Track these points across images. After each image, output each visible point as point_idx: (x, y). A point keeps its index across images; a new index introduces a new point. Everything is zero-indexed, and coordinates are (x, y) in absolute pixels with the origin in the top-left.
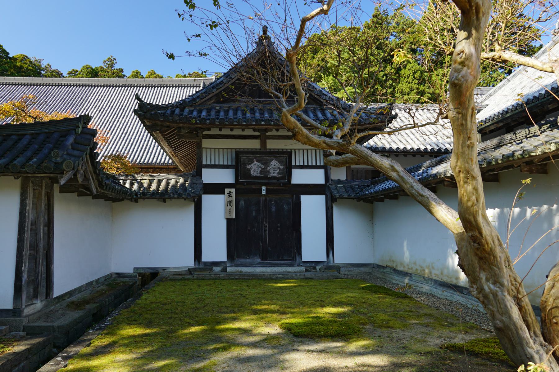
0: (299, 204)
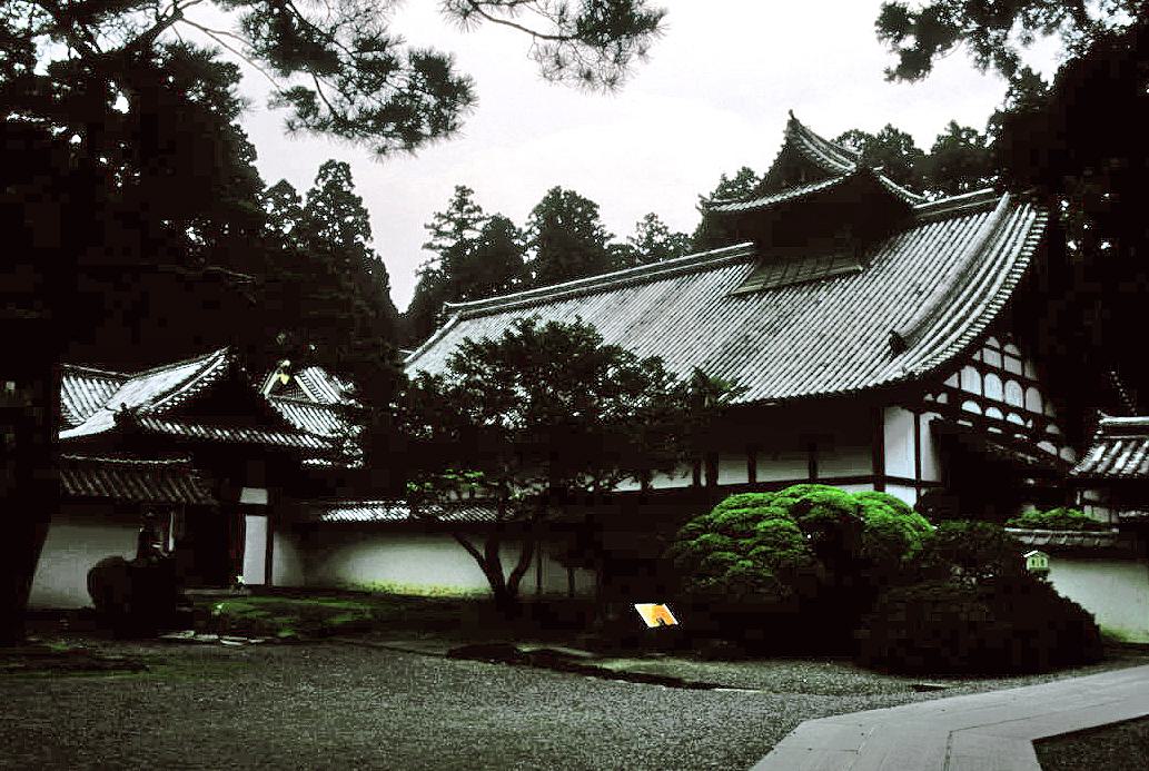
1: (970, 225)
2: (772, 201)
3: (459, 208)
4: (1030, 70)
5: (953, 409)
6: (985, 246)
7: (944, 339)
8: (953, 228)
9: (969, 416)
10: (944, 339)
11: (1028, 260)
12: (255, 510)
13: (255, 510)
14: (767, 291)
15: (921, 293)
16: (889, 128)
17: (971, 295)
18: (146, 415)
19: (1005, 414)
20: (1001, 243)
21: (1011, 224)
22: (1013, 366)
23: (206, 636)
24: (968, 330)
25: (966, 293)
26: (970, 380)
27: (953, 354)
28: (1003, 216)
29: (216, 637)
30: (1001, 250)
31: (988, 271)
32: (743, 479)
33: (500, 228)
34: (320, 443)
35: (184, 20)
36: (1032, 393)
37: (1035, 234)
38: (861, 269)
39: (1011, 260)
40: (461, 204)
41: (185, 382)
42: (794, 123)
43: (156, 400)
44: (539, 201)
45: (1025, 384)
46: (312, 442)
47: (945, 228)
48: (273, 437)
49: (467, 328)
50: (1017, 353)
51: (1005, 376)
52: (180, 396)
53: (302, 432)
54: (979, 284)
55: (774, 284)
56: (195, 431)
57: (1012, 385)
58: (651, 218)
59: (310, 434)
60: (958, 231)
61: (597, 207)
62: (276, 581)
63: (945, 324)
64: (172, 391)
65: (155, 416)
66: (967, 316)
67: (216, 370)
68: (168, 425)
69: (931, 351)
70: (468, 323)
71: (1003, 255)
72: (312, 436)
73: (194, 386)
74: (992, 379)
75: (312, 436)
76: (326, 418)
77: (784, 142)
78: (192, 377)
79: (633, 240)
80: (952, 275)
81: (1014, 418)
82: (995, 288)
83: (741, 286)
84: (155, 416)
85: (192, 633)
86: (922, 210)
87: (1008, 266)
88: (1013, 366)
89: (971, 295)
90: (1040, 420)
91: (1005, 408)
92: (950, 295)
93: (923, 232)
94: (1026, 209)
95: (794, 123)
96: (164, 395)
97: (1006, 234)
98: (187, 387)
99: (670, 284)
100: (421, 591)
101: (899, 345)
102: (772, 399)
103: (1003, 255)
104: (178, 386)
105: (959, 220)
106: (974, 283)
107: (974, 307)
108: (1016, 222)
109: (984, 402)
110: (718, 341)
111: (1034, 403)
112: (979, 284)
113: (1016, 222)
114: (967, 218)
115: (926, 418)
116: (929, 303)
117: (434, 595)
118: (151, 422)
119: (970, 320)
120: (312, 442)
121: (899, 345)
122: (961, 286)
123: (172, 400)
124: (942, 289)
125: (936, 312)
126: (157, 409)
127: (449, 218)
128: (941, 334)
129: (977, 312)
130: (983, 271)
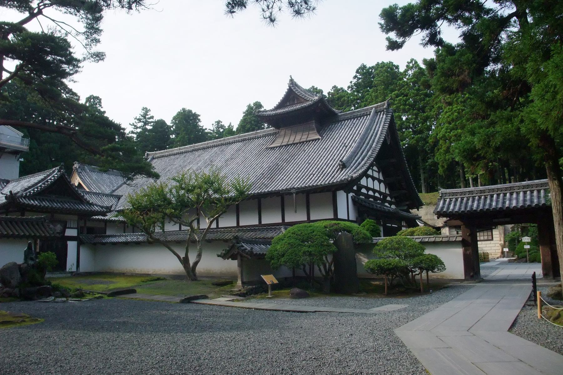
0: (67, 245)
1: (361, 120)
2: (284, 110)
3: (145, 117)
4: (195, 117)
5: (358, 192)
6: (369, 129)
7: (359, 164)
8: (354, 122)
9: (363, 194)
10: (359, 164)
11: (385, 133)
12: (72, 238)
13: (72, 238)
14: (288, 145)
15: (347, 147)
16: (313, 87)
17: (366, 147)
18: (21, 196)
19: (374, 193)
20: (374, 127)
21: (377, 120)
22: (376, 175)
23: (60, 299)
24: (367, 160)
25: (364, 146)
26: (363, 182)
27: (364, 169)
28: (373, 117)
29: (65, 299)
30: (375, 130)
31: (371, 138)
32: (277, 219)
33: (161, 124)
34: (101, 209)
35: (43, 30)
36: (382, 185)
37: (386, 126)
38: (320, 138)
39: (379, 133)
40: (144, 116)
41: (39, 182)
42: (292, 80)
43: (26, 189)
44: (175, 115)
45: (380, 181)
46: (97, 208)
47: (351, 123)
48: (80, 206)
49: (156, 162)
50: (377, 170)
51: (374, 179)
52: (37, 188)
53: (92, 204)
54: (368, 143)
55: (285, 144)
56: (44, 203)
57: (376, 182)
58: (218, 122)
59: (96, 205)
60: (356, 123)
61: (199, 116)
62: (82, 269)
63: (359, 158)
64: (33, 186)
65: (25, 197)
66: (366, 155)
67: (54, 177)
68: (32, 201)
69: (356, 168)
70: (156, 160)
71: (376, 131)
72: (97, 206)
73: (44, 184)
74: (370, 180)
75: (97, 206)
76: (99, 198)
77: (288, 88)
78: (43, 180)
79: (211, 130)
80: (358, 139)
81: (377, 195)
82: (375, 144)
83: (272, 143)
84: (25, 197)
85: (53, 298)
86: (341, 115)
87: (378, 135)
88: (376, 175)
89: (366, 147)
90: (385, 195)
91: (374, 191)
92: (359, 147)
93: (342, 123)
94: (382, 114)
95: (292, 80)
96: (30, 187)
97: (375, 123)
98: (40, 184)
99: (240, 144)
100: (148, 272)
101: (344, 166)
102: (294, 188)
103: (376, 131)
104: (37, 184)
105: (356, 119)
106: (366, 142)
107: (368, 151)
108: (379, 119)
109: (368, 189)
110: (265, 166)
111: (383, 189)
112: (368, 143)
113: (379, 119)
114: (359, 118)
115: (351, 195)
116: (351, 150)
117: (154, 273)
118: (24, 200)
119: (368, 156)
120: (97, 208)
121: (344, 166)
122: (362, 144)
123: (34, 190)
124: (354, 145)
125: (354, 154)
126: (26, 194)
127: (139, 120)
128: (358, 162)
129: (370, 153)
130: (369, 138)
